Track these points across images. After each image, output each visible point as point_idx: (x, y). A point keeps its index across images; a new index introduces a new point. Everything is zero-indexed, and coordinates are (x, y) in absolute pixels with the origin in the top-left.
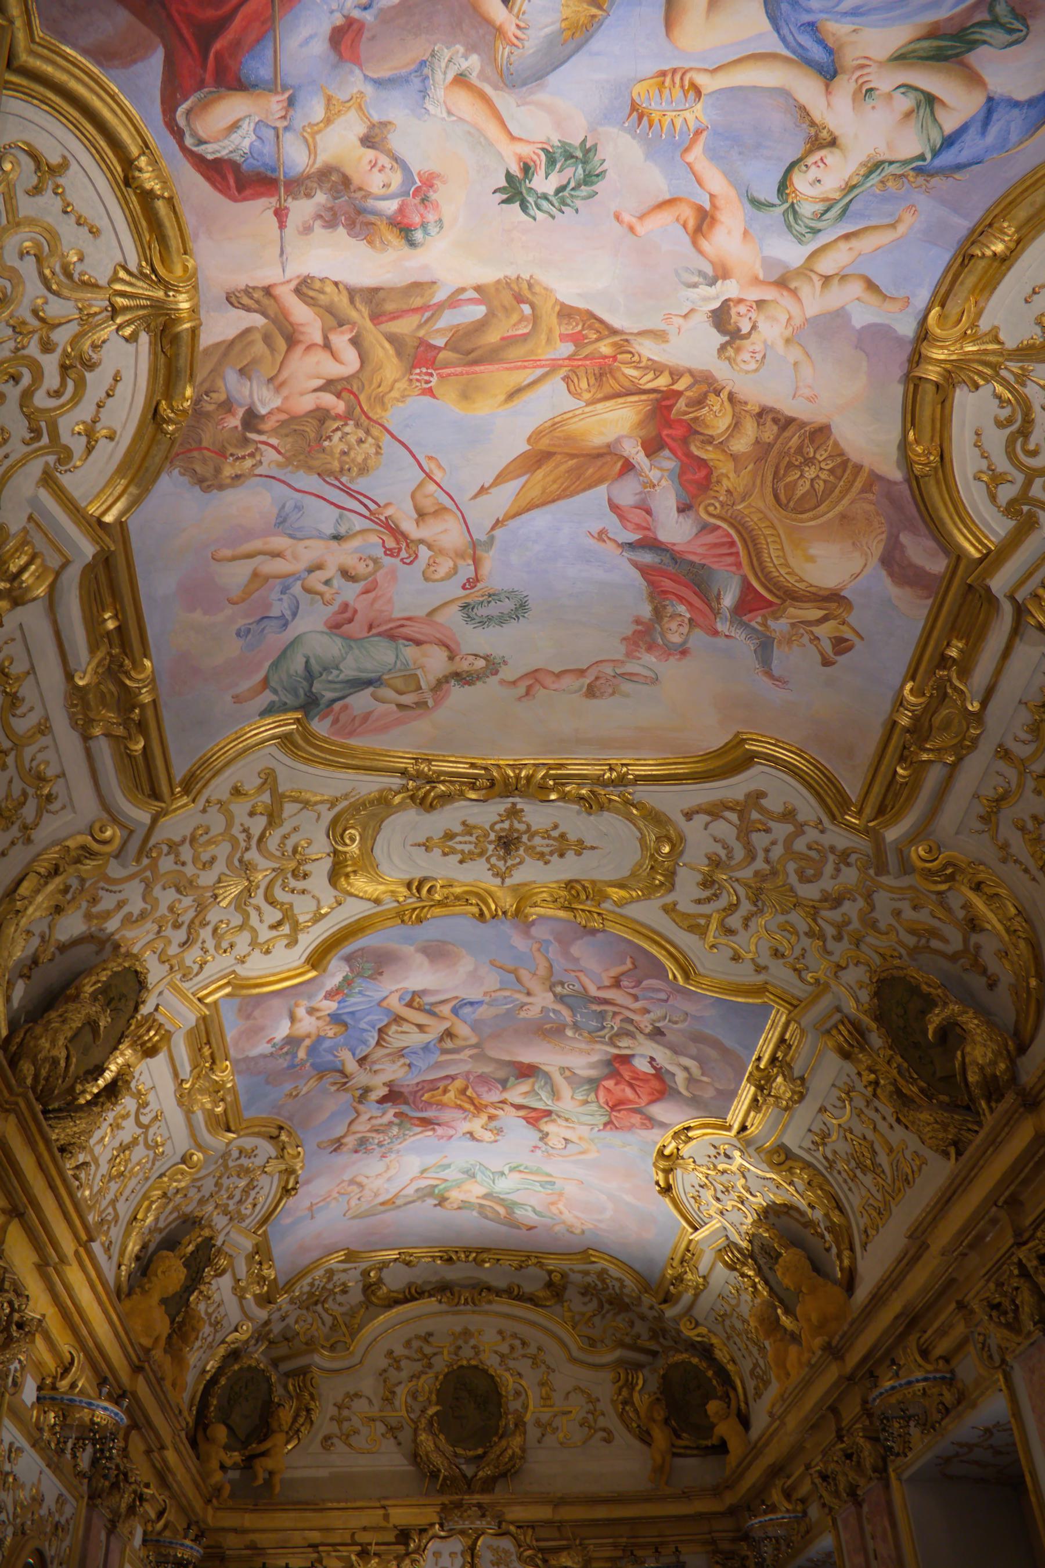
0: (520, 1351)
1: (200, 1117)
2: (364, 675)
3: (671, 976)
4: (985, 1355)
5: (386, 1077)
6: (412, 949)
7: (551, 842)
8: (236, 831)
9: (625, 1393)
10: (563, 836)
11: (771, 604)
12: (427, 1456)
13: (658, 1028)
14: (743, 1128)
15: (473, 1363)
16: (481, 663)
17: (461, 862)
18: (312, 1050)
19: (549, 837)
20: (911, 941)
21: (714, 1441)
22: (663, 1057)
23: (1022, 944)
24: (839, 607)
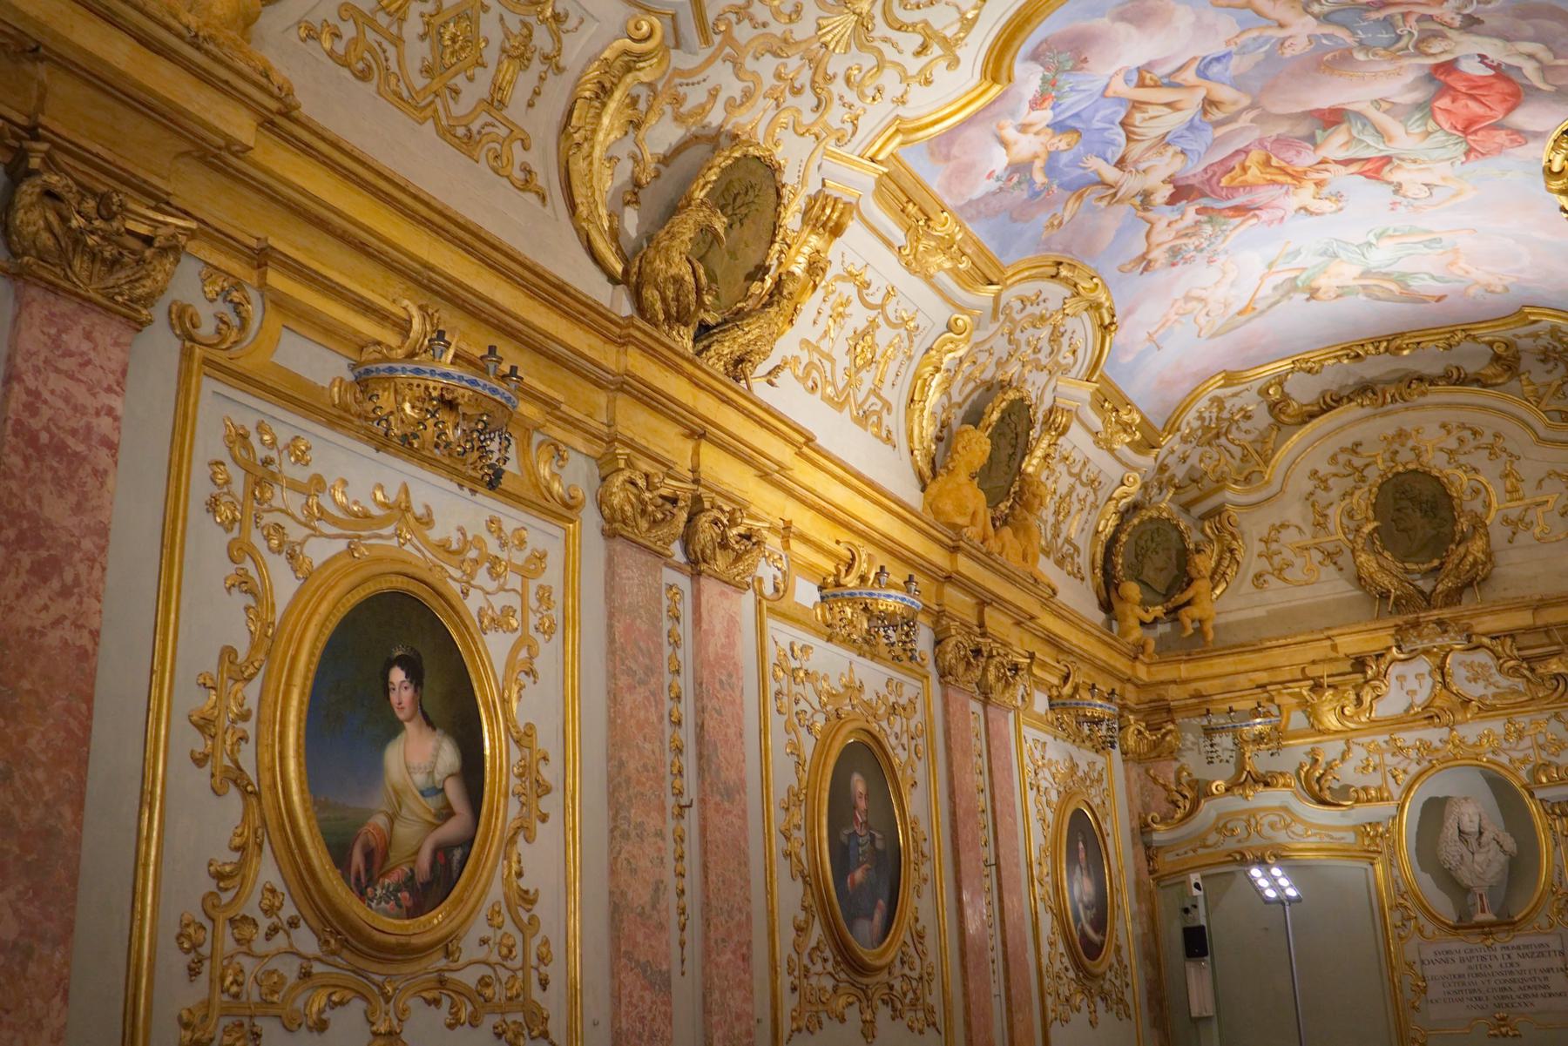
0: (1471, 443)
6: (1106, 20)
13: (1469, 16)
15: (1411, 466)
18: (1051, 169)
22: (1495, 50)
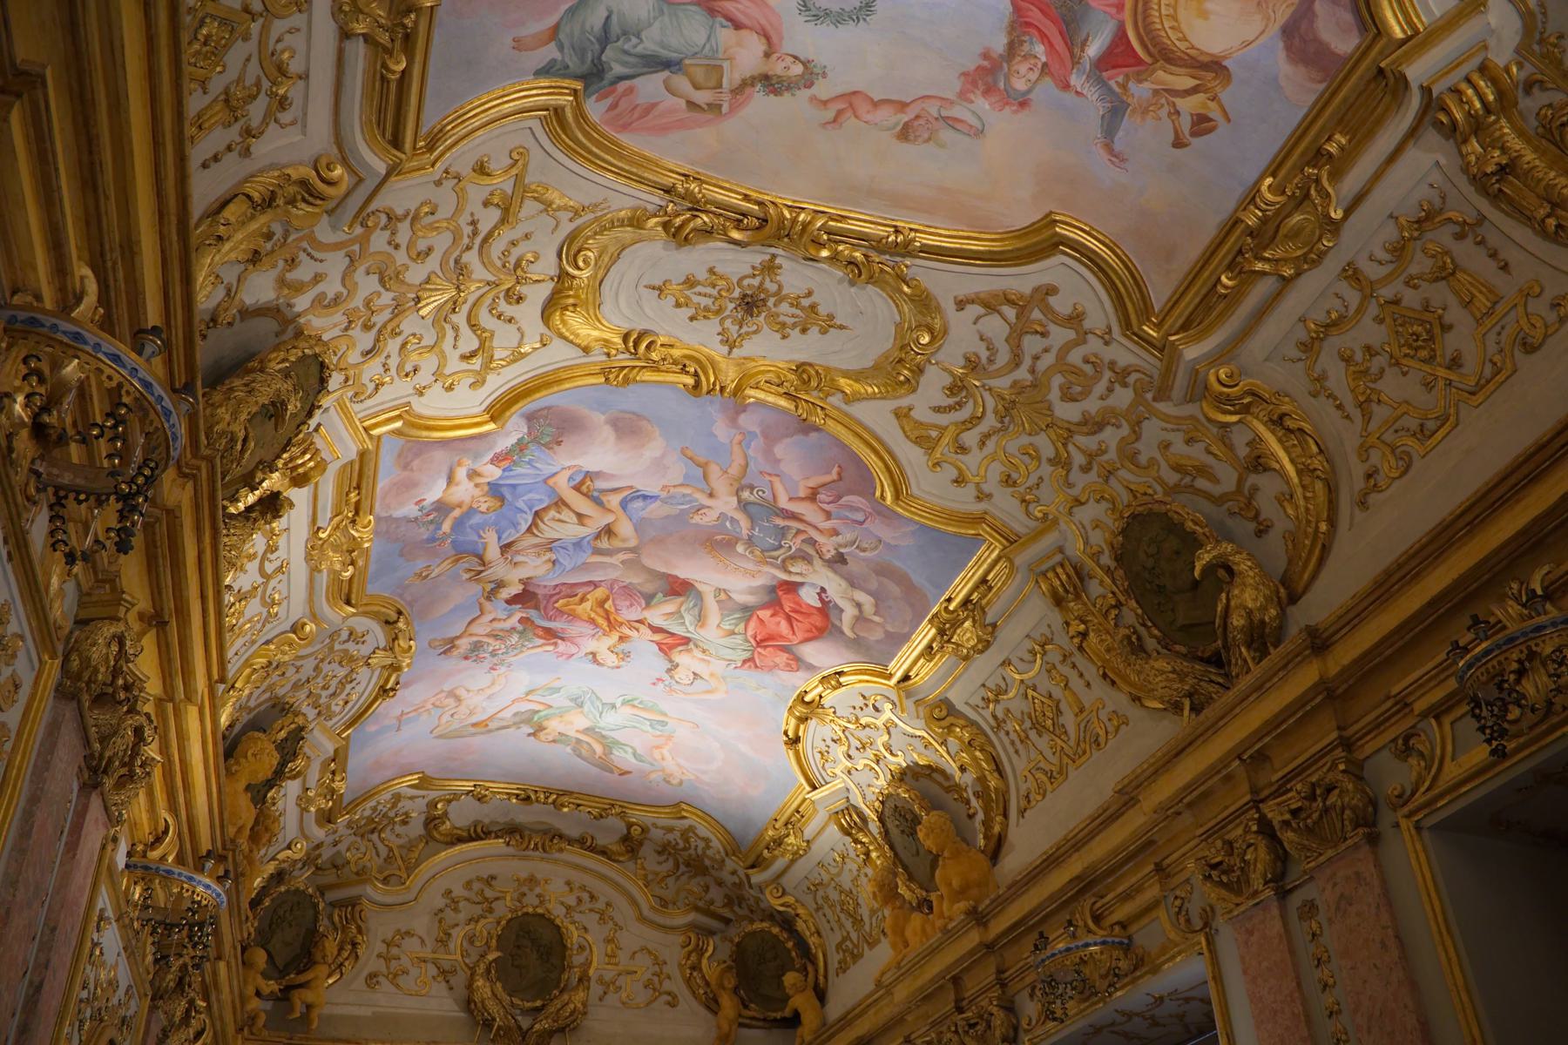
0: (587, 905)
1: (323, 579)
2: (665, 53)
3: (878, 494)
4: (1182, 920)
5: (523, 573)
6: (603, 418)
7: (798, 312)
8: (464, 220)
9: (694, 957)
10: (813, 307)
11: (1140, 62)
12: (483, 1002)
14: (906, 678)
15: (540, 911)
16: (798, 69)
17: (692, 319)
18: (459, 524)
19: (797, 306)
20: (1172, 478)
21: (787, 1013)
22: (836, 588)
23: (1319, 485)
24: (1214, 79)
